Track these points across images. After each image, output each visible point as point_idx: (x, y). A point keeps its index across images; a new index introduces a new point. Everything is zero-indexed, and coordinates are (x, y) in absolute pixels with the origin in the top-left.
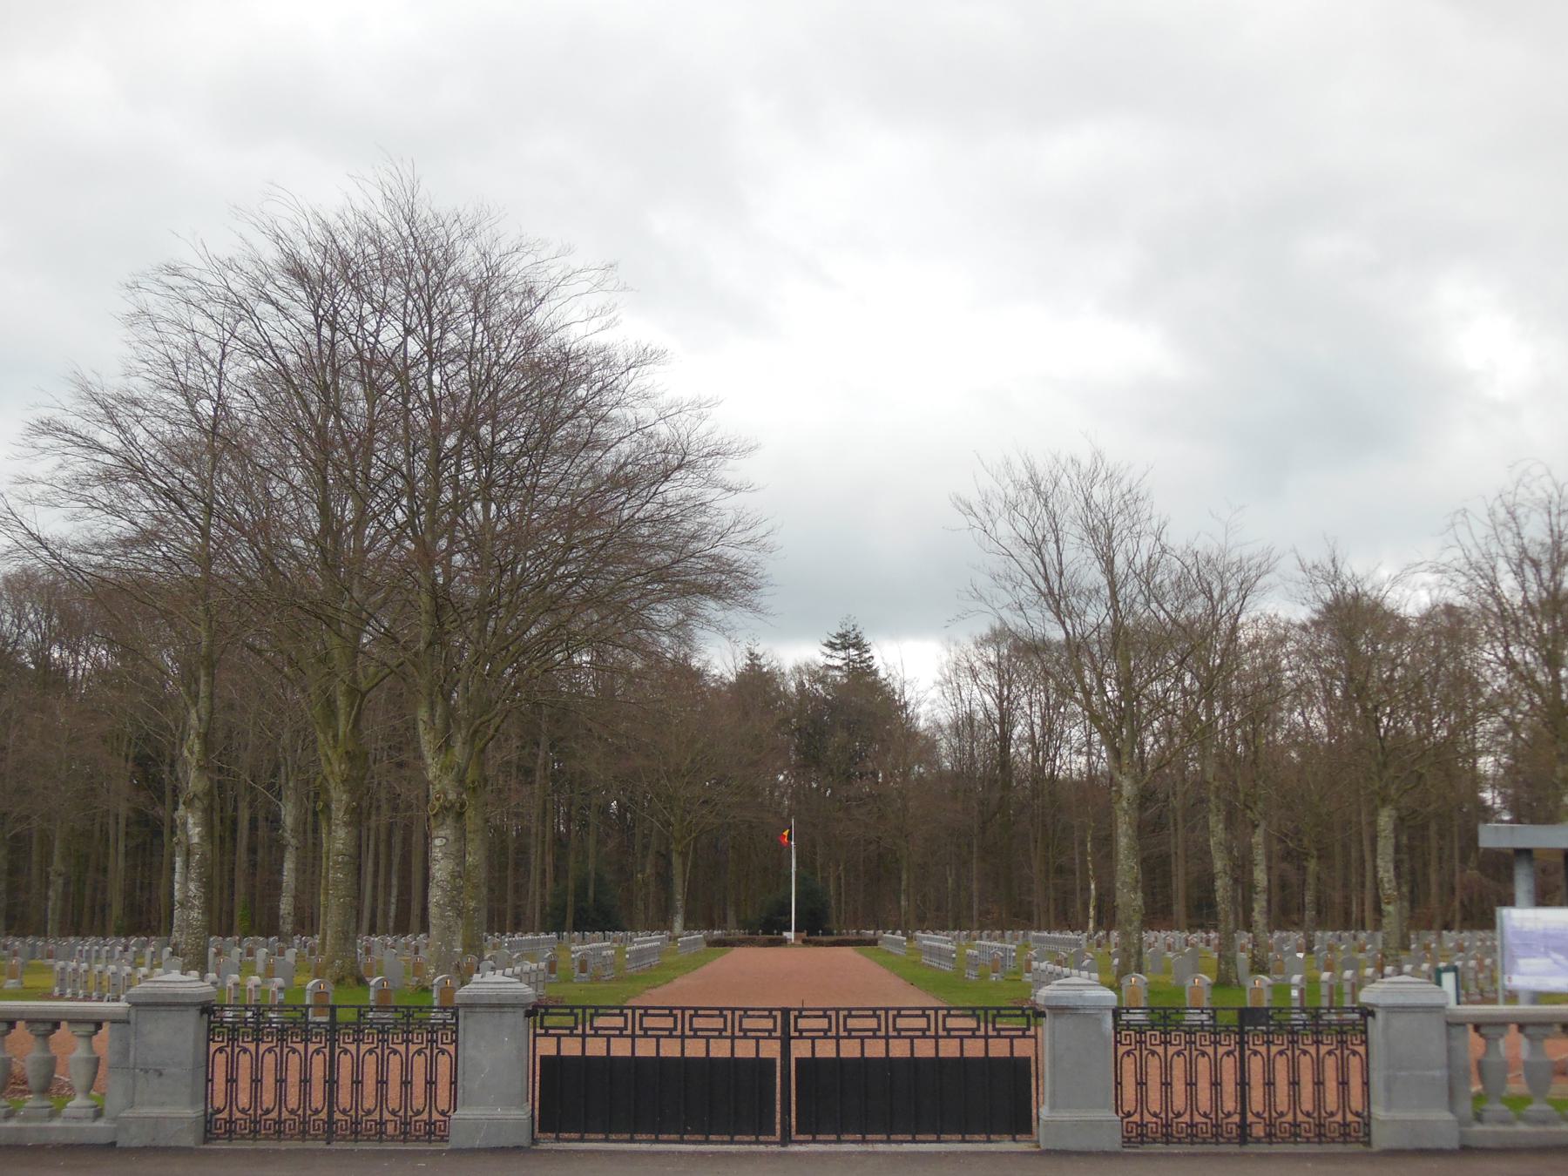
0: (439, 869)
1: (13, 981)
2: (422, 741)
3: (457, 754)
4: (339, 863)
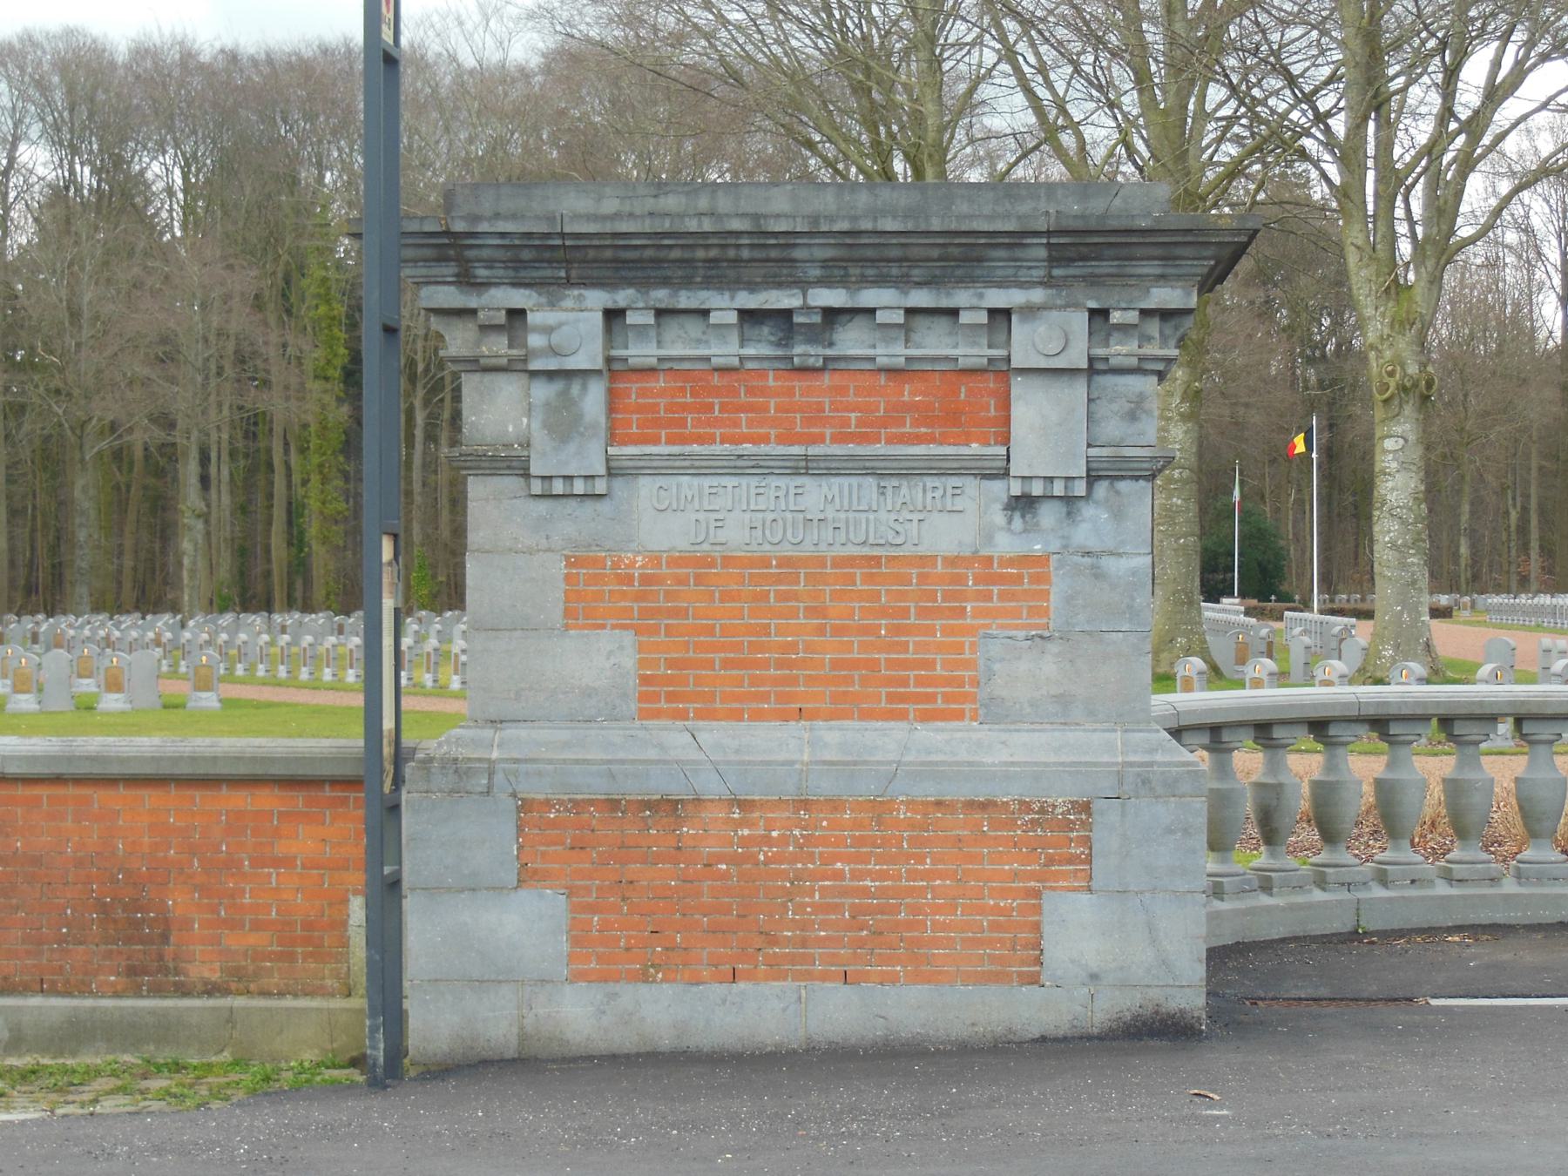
0: (1393, 489)
1: (116, 696)
2: (1354, 279)
3: (1418, 299)
4: (1176, 481)
